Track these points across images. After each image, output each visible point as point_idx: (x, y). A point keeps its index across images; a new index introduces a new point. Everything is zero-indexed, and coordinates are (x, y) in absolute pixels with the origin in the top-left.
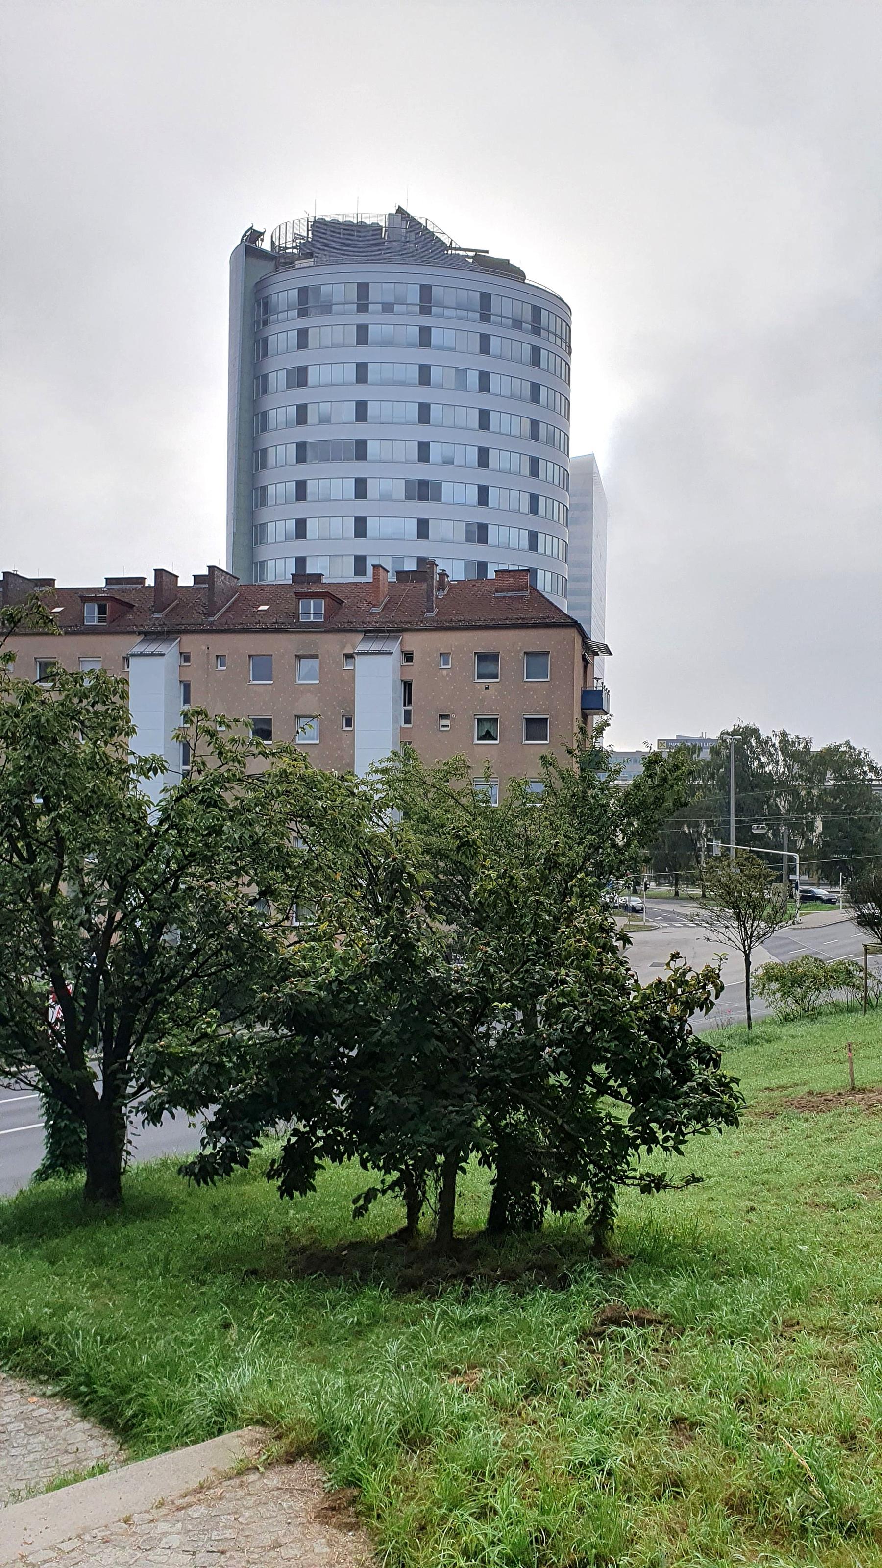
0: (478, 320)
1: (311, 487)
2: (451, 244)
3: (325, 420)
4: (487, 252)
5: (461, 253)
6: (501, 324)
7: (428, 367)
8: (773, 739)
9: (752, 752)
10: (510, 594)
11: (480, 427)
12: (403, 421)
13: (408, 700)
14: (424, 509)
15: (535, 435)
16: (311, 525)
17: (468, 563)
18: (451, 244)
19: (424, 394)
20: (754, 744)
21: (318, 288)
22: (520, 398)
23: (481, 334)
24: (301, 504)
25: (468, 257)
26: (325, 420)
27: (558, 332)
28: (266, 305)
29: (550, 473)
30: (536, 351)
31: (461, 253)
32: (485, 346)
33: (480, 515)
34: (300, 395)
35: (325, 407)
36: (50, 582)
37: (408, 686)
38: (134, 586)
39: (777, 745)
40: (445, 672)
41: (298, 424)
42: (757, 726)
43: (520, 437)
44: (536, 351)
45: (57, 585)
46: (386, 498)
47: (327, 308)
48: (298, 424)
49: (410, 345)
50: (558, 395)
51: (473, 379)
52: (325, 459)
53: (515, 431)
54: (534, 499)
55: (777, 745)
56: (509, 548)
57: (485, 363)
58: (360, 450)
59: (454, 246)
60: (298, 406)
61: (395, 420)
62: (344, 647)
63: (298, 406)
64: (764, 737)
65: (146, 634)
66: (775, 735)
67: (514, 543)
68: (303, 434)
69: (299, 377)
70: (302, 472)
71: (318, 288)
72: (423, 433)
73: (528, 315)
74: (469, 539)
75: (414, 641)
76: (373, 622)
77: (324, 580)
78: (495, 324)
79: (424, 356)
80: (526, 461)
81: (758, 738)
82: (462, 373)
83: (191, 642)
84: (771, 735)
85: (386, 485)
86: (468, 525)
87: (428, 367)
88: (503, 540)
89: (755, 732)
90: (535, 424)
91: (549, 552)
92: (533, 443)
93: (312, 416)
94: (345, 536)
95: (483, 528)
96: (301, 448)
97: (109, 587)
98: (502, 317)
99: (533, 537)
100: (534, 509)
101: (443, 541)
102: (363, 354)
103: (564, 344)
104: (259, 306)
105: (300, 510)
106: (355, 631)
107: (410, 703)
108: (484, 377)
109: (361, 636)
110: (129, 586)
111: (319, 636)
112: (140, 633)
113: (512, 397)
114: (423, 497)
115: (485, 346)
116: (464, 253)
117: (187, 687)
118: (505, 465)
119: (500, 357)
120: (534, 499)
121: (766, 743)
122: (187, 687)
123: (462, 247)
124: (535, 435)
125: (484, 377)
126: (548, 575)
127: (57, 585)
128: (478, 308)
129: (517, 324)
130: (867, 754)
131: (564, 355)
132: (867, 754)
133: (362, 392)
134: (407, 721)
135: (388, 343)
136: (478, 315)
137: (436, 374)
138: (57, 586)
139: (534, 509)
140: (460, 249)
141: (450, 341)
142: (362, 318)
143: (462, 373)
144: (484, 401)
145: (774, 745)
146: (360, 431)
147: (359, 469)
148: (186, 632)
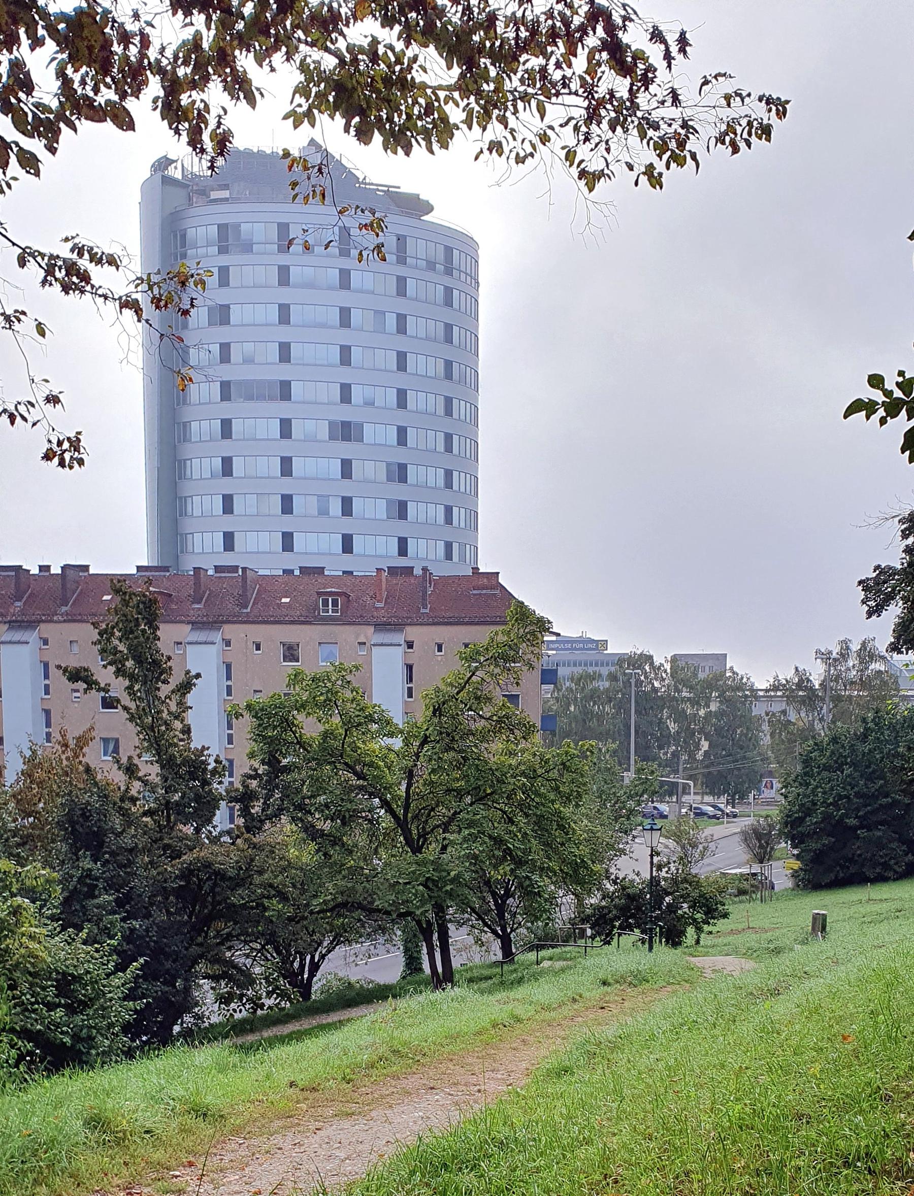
0: (395, 262)
1: (236, 426)
2: (365, 179)
3: (248, 360)
4: (399, 188)
5: (372, 187)
6: (416, 267)
7: (348, 310)
8: (665, 665)
9: (646, 677)
10: (484, 592)
11: (398, 369)
12: (325, 363)
13: (410, 679)
14: (346, 449)
15: (449, 375)
16: (237, 464)
17: (389, 502)
18: (365, 179)
19: (345, 337)
20: (648, 670)
21: (237, 226)
22: (435, 340)
23: (398, 277)
24: (227, 442)
25: (378, 190)
26: (248, 360)
27: (468, 272)
28: (184, 236)
29: (463, 411)
30: (449, 291)
31: (372, 187)
32: (401, 290)
33: (400, 456)
34: (223, 334)
35: (249, 347)
36: (86, 568)
37: (410, 668)
38: (162, 573)
39: (669, 671)
40: (439, 658)
41: (221, 363)
42: (651, 653)
43: (435, 378)
44: (449, 291)
45: (92, 571)
46: (311, 439)
47: (248, 248)
48: (221, 363)
49: (331, 288)
50: (468, 333)
51: (391, 321)
52: (250, 398)
53: (431, 373)
54: (448, 438)
55: (669, 671)
56: (427, 487)
57: (402, 305)
58: (285, 391)
59: (367, 181)
60: (221, 345)
61: (318, 362)
62: (357, 638)
63: (221, 345)
64: (657, 664)
65: (193, 623)
66: (667, 661)
67: (431, 483)
68: (227, 372)
69: (221, 315)
70: (227, 410)
71: (237, 226)
72: (345, 375)
73: (441, 257)
74: (389, 479)
75: (412, 633)
76: (382, 616)
77: (326, 573)
78: (411, 267)
79: (344, 298)
80: (441, 401)
81: (652, 664)
82: (380, 314)
83: (230, 630)
84: (663, 662)
85: (310, 425)
86: (388, 465)
87: (348, 310)
88: (422, 479)
89: (650, 658)
90: (449, 364)
91: (463, 489)
92: (446, 383)
93: (236, 354)
94: (272, 475)
95: (403, 468)
96: (226, 387)
97: (139, 574)
98: (417, 259)
99: (449, 474)
100: (449, 448)
101: (365, 481)
102: (285, 295)
103: (468, 278)
104: (175, 236)
105: (226, 448)
106: (368, 624)
107: (411, 680)
108: (401, 319)
109: (372, 629)
110: (157, 573)
111: (338, 627)
112: (188, 623)
113: (427, 338)
114: (346, 437)
115: (401, 290)
116: (375, 187)
117: (229, 667)
118: (422, 406)
119: (416, 299)
120: (448, 438)
121: (659, 668)
122: (229, 667)
123: (374, 182)
124: (449, 375)
125: (401, 319)
126: (463, 510)
127: (92, 571)
128: (395, 251)
129: (431, 266)
130: (748, 679)
131: (472, 292)
132: (748, 679)
133: (284, 334)
134: (410, 696)
135: (310, 285)
136: (395, 257)
137: (356, 317)
138: (92, 571)
139: (449, 448)
140: (372, 184)
141: (369, 284)
142: (284, 260)
143: (380, 314)
144: (402, 343)
145: (665, 671)
146: (283, 372)
147: (284, 409)
148: (228, 622)
